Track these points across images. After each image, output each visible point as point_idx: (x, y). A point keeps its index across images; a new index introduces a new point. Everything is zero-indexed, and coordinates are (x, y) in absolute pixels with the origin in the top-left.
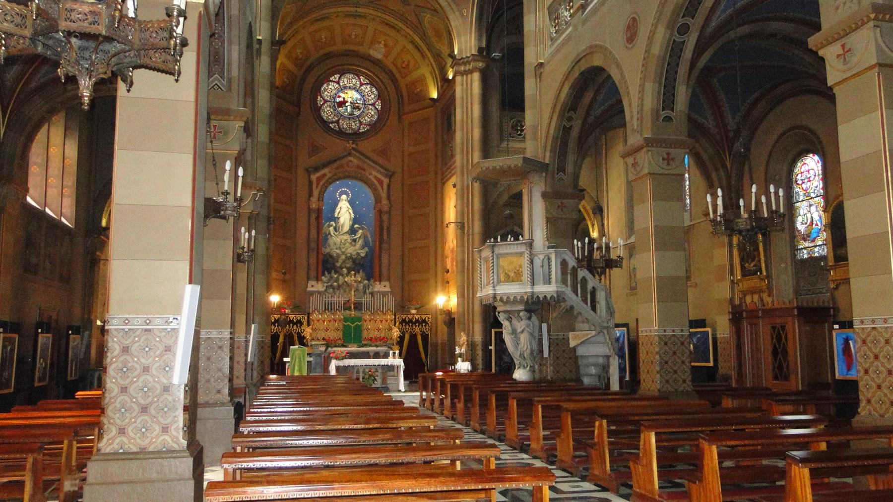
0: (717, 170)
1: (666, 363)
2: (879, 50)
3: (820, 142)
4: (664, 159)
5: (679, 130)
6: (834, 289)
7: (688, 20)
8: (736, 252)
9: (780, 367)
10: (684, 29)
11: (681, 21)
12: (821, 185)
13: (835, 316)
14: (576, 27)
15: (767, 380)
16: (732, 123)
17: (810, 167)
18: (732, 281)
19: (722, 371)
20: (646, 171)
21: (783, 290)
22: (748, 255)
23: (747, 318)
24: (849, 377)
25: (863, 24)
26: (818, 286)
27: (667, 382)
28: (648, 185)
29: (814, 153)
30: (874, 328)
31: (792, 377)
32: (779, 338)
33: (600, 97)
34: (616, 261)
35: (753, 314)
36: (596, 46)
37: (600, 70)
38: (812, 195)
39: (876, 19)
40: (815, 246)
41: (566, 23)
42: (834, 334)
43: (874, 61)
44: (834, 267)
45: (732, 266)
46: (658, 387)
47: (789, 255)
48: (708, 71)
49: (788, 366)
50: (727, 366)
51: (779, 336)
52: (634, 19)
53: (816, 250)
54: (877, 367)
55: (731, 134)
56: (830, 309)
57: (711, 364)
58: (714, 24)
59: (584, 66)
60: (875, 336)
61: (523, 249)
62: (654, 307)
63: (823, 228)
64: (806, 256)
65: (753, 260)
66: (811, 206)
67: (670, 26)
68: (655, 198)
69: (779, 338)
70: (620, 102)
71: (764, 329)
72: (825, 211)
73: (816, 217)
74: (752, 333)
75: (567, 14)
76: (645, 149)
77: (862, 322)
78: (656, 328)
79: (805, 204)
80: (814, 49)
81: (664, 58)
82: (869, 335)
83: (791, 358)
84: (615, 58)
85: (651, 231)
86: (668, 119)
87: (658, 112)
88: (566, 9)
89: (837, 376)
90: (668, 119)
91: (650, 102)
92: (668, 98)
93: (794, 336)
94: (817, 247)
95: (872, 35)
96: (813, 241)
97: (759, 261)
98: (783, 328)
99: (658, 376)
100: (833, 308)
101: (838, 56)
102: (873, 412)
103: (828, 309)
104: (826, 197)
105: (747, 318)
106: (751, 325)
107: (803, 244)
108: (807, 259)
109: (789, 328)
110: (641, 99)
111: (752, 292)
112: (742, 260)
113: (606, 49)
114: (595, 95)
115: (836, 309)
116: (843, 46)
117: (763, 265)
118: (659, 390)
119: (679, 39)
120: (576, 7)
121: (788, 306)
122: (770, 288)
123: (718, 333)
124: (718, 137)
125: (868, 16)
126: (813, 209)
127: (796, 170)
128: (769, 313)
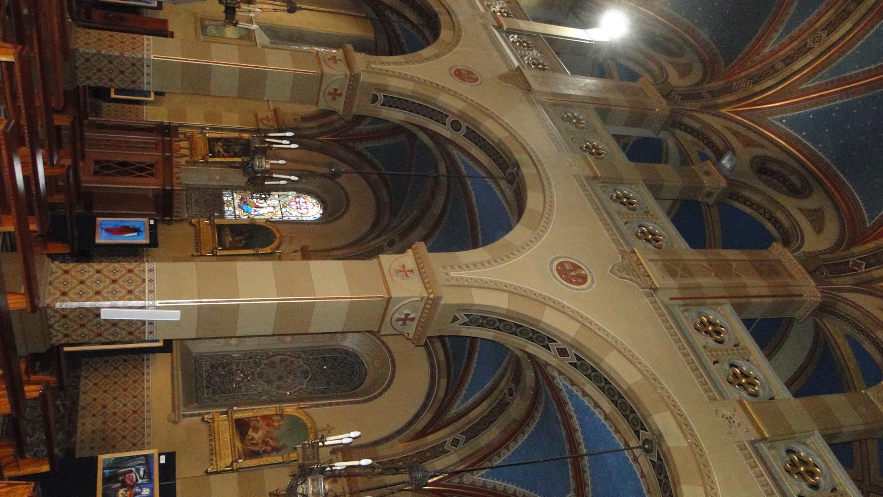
0: (320, 126)
1: (110, 62)
2: (401, 299)
3: (332, 221)
4: (336, 90)
5: (363, 105)
6: (191, 222)
7: (463, 130)
8: (236, 135)
9: (108, 168)
10: (456, 126)
11: (464, 125)
12: (292, 219)
13: (163, 221)
14: (482, 16)
15: (94, 153)
16: (361, 147)
17: (309, 210)
18: (203, 128)
19: (105, 105)
20: (326, 70)
21: (192, 176)
22: (230, 146)
23: (163, 140)
24: (98, 230)
25: (427, 289)
26: (194, 208)
27: (87, 60)
28: (312, 71)
29: (325, 209)
30: (144, 281)
31: (96, 178)
32: (142, 169)
33: (408, 27)
34: (233, 19)
35: (168, 147)
36: (459, 36)
37: (436, 36)
38: (284, 210)
39: (428, 298)
40: (234, 208)
41: (489, 6)
42: (144, 220)
43: (394, 295)
44: (212, 224)
45: (221, 129)
46: (81, 50)
47: (228, 184)
48: (412, 137)
49: (108, 175)
50: (110, 113)
51: (143, 170)
52: (476, 80)
53: (231, 209)
54: (104, 282)
55: (351, 144)
56: (171, 216)
57: (113, 96)
58: (455, 152)
59: (443, 18)
60: (136, 281)
61: (225, 461)
62: (177, 58)
63: (252, 217)
64: (225, 199)
65: (225, 151)
66: (274, 207)
67: (462, 115)
68: (296, 76)
69: (142, 169)
70: (403, 52)
71: (151, 156)
72: (267, 220)
73: (261, 211)
74: (147, 143)
75: (498, 8)
76: (348, 73)
77: (151, 270)
78: (152, 57)
79: (276, 203)
80: (413, 246)
81: (435, 105)
82: (137, 275)
83: (120, 179)
84: (445, 54)
85: (262, 67)
86: (375, 99)
87: (385, 91)
88: (502, 8)
89: (99, 219)
90: (375, 99)
91: (395, 84)
92: (394, 102)
93: (141, 184)
94: (236, 208)
95: (417, 295)
96: (240, 207)
97: (223, 156)
98: (152, 175)
99: (94, 51)
100: (171, 220)
101: (404, 266)
102: (54, 276)
103: (170, 215)
104: (282, 222)
105: (163, 140)
106: (156, 144)
107: (237, 197)
108: (222, 200)
109: (152, 180)
110: (401, 76)
111: (192, 149)
112: (226, 140)
113: (455, 46)
114: (414, 26)
115: (169, 223)
116: (412, 271)
117: (218, 160)
118: (76, 49)
119: (448, 121)
120: (502, 20)
121: (175, 181)
122: (195, 163)
123: (149, 107)
124: (351, 132)
125: (432, 293)
126: (271, 209)
127: (309, 198)
128: (168, 162)
